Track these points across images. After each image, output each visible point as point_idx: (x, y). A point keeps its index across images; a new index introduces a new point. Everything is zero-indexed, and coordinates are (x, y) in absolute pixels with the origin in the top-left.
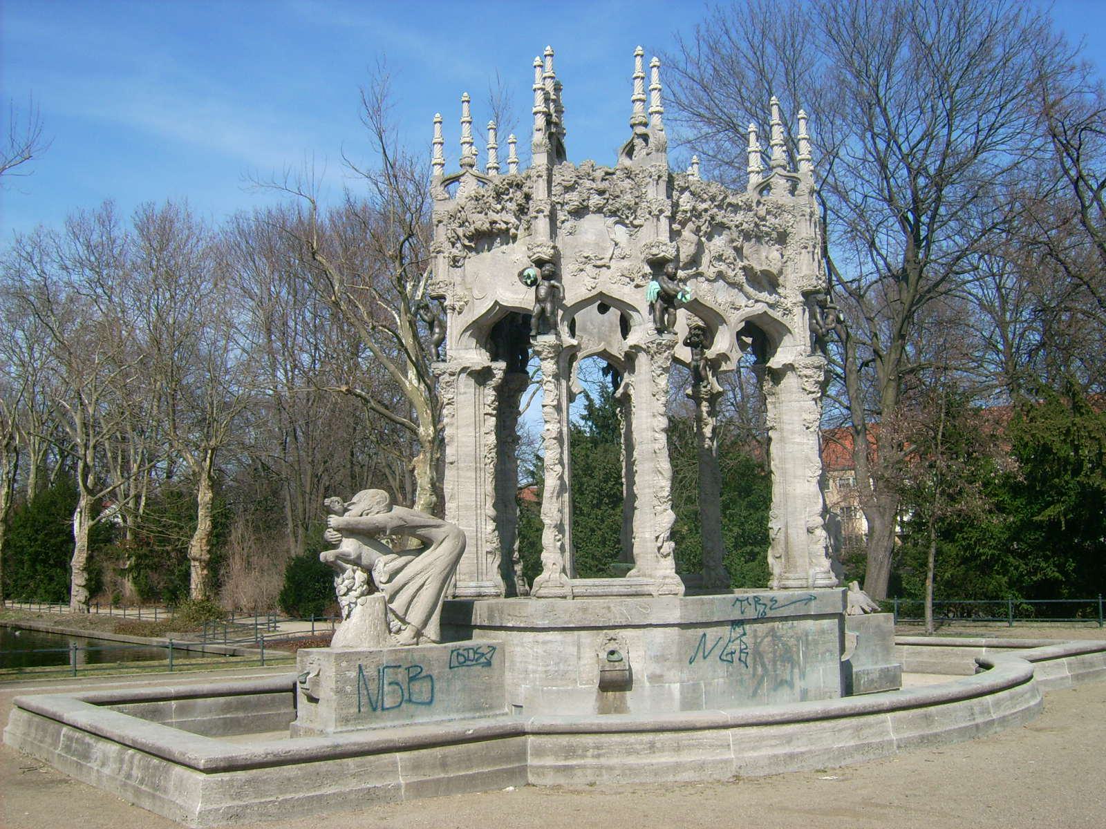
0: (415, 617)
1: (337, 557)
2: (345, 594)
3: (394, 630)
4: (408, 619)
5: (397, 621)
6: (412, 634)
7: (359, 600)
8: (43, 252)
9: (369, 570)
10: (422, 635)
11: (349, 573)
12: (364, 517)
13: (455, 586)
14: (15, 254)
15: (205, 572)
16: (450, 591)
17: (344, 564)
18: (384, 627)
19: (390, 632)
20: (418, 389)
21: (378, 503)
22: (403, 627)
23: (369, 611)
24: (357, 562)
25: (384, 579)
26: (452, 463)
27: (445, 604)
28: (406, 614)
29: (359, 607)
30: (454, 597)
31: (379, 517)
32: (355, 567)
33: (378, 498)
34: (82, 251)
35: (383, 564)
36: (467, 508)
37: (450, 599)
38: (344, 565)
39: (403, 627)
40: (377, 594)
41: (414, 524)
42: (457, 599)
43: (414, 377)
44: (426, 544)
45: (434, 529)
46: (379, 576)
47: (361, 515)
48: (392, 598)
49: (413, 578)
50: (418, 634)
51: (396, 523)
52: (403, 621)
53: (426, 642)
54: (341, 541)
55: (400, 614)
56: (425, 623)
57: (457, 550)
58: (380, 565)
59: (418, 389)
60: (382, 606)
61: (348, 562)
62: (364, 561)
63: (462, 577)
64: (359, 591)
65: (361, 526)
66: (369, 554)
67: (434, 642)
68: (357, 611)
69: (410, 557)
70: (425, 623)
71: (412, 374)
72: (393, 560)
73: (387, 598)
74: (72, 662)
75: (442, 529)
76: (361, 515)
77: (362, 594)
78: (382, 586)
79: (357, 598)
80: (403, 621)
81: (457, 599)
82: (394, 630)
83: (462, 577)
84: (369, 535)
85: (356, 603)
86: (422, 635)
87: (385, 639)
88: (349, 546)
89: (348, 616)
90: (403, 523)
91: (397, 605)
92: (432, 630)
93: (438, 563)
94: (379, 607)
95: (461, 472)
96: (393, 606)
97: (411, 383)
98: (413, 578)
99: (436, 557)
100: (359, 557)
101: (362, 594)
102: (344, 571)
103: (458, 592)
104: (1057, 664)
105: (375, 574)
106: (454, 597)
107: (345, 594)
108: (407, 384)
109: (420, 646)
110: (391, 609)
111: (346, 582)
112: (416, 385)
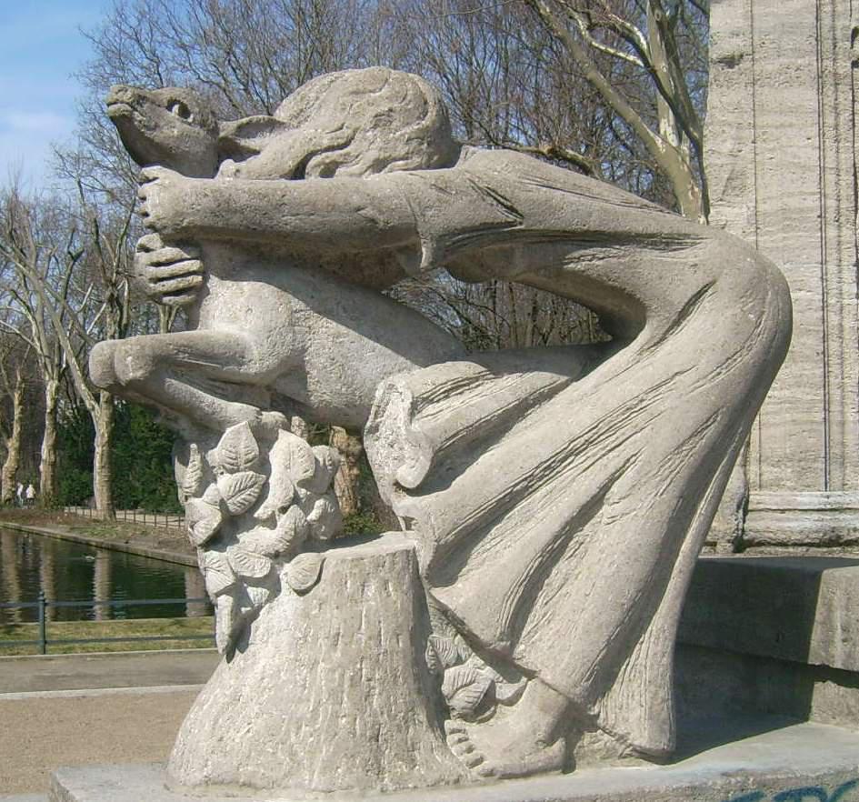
0: (559, 644)
1: (164, 364)
2: (216, 541)
3: (460, 701)
4: (526, 653)
5: (474, 661)
6: (545, 722)
7: (289, 572)
8: (153, 25)
9: (342, 423)
10: (592, 724)
11: (236, 440)
12: (313, 182)
13: (744, 506)
14: (114, 29)
15: (355, 471)
16: (724, 525)
17: (208, 400)
18: (403, 691)
19: (439, 710)
20: (677, 150)
21: (382, 120)
22: (505, 690)
23: (333, 618)
24: (282, 392)
25: (411, 473)
26: (730, 62)
27: (703, 573)
28: (515, 628)
29: (287, 601)
30: (740, 544)
31: (383, 183)
32: (272, 417)
33: (381, 99)
34: (206, 20)
35: (411, 399)
36: (788, 218)
37: (723, 552)
38: (208, 400)
39: (505, 690)
40: (390, 542)
41: (552, 223)
42: (750, 554)
43: (670, 130)
44: (606, 325)
45: (648, 255)
46: (397, 458)
47: (299, 172)
48: (453, 556)
49: (549, 469)
50: (573, 722)
51: (462, 212)
52: (505, 663)
53: (609, 755)
54: (200, 292)
55: (488, 632)
56: (604, 675)
57: (758, 345)
58: (398, 408)
59: (677, 150)
60: (398, 597)
61: (238, 389)
62: (322, 389)
63: (769, 473)
64: (285, 523)
65: (289, 221)
66: (339, 353)
67: (645, 755)
68: (278, 620)
69: (540, 379)
70: (604, 675)
71: (667, 125)
72: (457, 387)
73: (425, 559)
74: (41, 617)
75: (687, 255)
76: (299, 172)
77: (306, 541)
78: (402, 505)
79: (278, 557)
80: (505, 663)
81: (750, 554)
82: (460, 701)
83: (769, 473)
84: (353, 267)
85: (272, 584)
86: (592, 724)
87: (408, 754)
88: (241, 315)
89: (239, 639)
90: (501, 215)
91: (476, 591)
92: (638, 703)
93: (666, 402)
94: (383, 604)
95: (766, 95)
96: (455, 596)
97: (665, 140)
98: (549, 469)
99: (651, 388)
100: (294, 368)
101: (306, 541)
102: (209, 431)
103: (757, 525)
104: (789, 505)
105: (377, 450)
106: (740, 544)
107: (216, 541)
108: (659, 142)
109: (581, 774)
110: (444, 611)
111: (224, 483)
112: (675, 144)
